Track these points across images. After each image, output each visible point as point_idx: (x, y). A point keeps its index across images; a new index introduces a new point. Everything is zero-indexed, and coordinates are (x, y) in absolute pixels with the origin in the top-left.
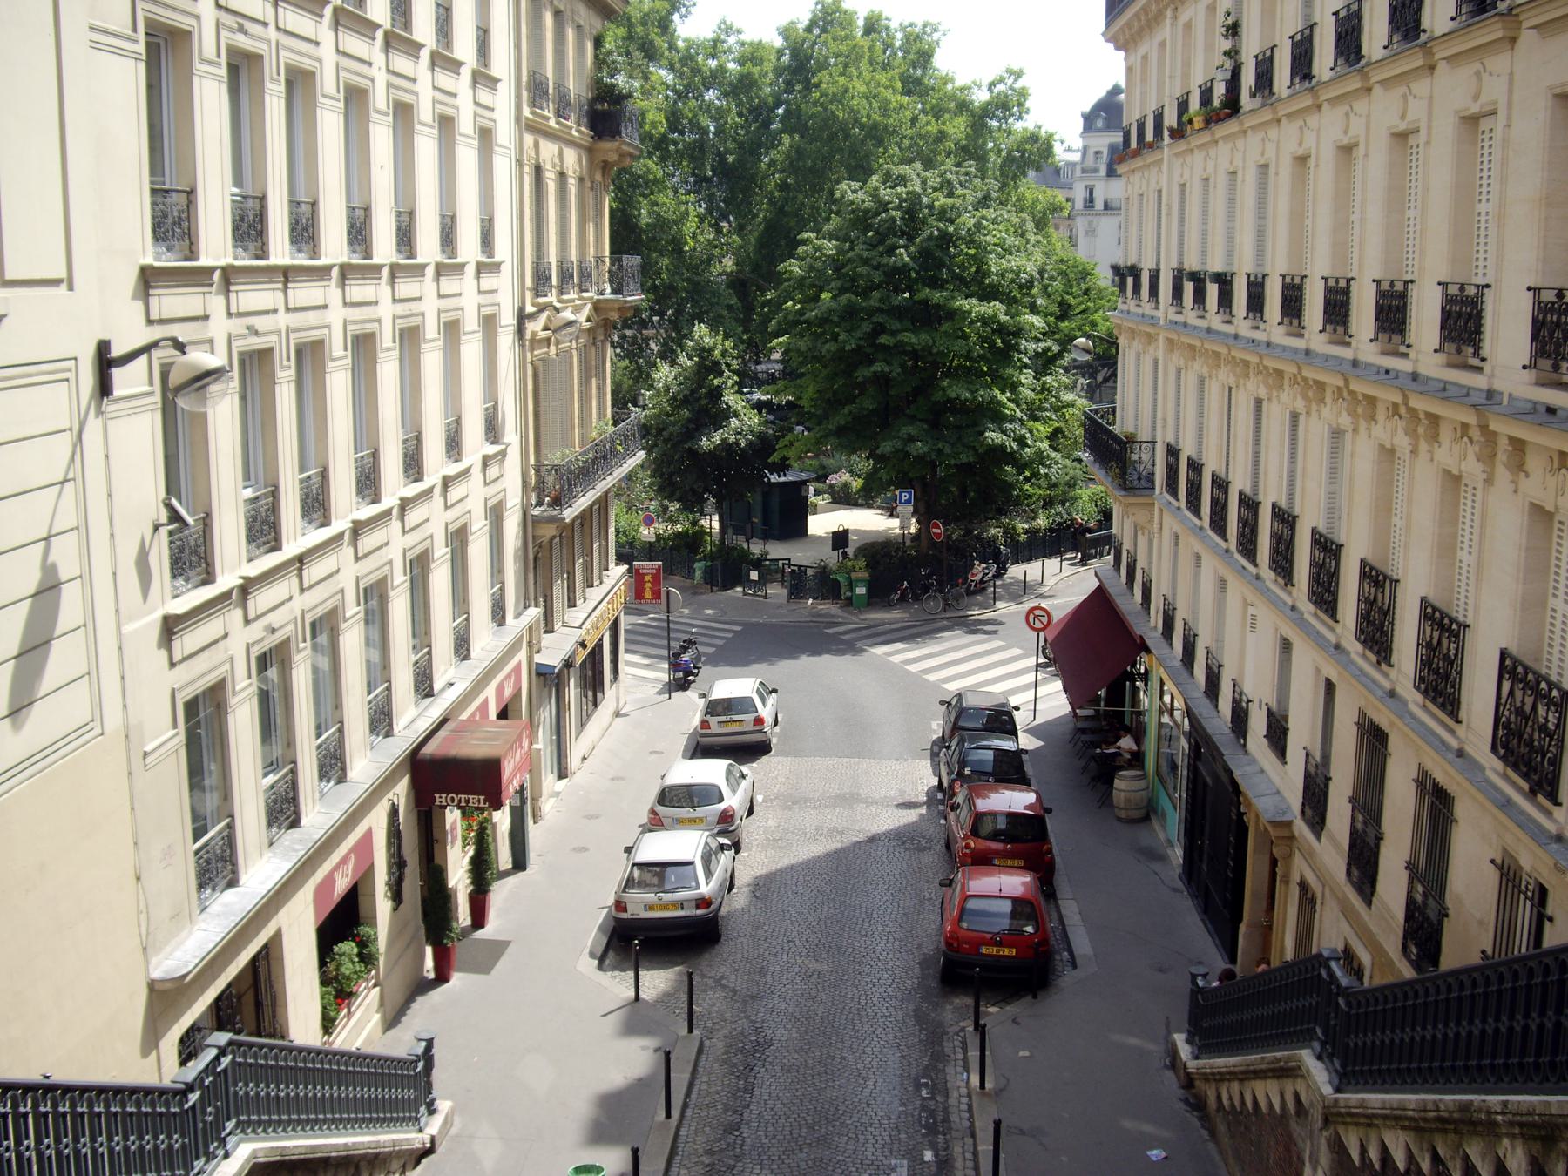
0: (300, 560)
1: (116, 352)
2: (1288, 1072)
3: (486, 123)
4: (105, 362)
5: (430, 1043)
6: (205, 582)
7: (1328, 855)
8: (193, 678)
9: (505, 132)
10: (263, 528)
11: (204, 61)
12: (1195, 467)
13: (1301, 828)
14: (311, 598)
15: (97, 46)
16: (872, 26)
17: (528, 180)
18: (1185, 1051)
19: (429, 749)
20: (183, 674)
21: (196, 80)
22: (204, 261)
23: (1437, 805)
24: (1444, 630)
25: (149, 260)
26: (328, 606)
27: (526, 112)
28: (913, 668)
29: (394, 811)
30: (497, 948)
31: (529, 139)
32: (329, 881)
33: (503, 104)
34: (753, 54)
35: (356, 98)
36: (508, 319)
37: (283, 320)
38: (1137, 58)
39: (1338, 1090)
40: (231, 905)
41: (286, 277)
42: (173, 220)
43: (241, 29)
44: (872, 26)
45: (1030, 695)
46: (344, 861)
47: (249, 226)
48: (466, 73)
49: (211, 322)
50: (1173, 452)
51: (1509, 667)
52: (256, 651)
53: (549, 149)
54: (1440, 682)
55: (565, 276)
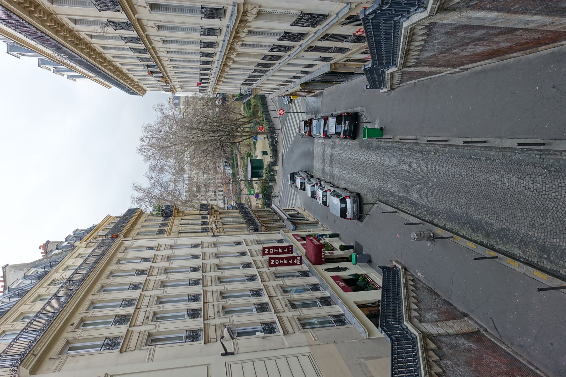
0: (270, 297)
1: (224, 352)
2: (392, 74)
3: (169, 247)
4: (226, 353)
5: (380, 267)
6: (276, 323)
7: (338, 57)
8: (296, 325)
9: (171, 241)
10: (262, 308)
11: (155, 328)
12: (246, 80)
13: (332, 62)
14: (279, 294)
15: (152, 359)
16: (142, 140)
17: (182, 235)
18: (385, 90)
19: (313, 260)
20: (296, 330)
21: (160, 330)
22: (202, 307)
23: (327, 37)
24: (286, 36)
25: (203, 342)
26: (280, 288)
27: (166, 236)
28: (293, 139)
29: (327, 270)
30: (357, 243)
31: (172, 234)
32: (343, 288)
33: (165, 241)
34: (152, 169)
35: (163, 284)
36: (214, 239)
37: (215, 303)
38: (148, 89)
39: (397, 66)
40: (349, 316)
41: (207, 303)
42: (193, 336)
43: (148, 318)
44: (142, 140)
45: (300, 114)
46: (338, 284)
47: (194, 314)
48: (157, 253)
49: (217, 323)
50: (243, 84)
51: (295, 24)
52: (291, 309)
53: (175, 229)
54: (298, 37)
55: (204, 223)
